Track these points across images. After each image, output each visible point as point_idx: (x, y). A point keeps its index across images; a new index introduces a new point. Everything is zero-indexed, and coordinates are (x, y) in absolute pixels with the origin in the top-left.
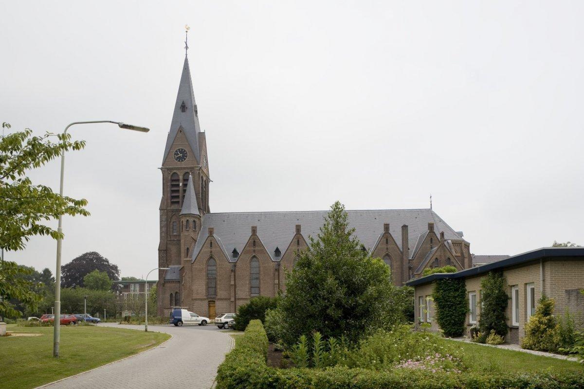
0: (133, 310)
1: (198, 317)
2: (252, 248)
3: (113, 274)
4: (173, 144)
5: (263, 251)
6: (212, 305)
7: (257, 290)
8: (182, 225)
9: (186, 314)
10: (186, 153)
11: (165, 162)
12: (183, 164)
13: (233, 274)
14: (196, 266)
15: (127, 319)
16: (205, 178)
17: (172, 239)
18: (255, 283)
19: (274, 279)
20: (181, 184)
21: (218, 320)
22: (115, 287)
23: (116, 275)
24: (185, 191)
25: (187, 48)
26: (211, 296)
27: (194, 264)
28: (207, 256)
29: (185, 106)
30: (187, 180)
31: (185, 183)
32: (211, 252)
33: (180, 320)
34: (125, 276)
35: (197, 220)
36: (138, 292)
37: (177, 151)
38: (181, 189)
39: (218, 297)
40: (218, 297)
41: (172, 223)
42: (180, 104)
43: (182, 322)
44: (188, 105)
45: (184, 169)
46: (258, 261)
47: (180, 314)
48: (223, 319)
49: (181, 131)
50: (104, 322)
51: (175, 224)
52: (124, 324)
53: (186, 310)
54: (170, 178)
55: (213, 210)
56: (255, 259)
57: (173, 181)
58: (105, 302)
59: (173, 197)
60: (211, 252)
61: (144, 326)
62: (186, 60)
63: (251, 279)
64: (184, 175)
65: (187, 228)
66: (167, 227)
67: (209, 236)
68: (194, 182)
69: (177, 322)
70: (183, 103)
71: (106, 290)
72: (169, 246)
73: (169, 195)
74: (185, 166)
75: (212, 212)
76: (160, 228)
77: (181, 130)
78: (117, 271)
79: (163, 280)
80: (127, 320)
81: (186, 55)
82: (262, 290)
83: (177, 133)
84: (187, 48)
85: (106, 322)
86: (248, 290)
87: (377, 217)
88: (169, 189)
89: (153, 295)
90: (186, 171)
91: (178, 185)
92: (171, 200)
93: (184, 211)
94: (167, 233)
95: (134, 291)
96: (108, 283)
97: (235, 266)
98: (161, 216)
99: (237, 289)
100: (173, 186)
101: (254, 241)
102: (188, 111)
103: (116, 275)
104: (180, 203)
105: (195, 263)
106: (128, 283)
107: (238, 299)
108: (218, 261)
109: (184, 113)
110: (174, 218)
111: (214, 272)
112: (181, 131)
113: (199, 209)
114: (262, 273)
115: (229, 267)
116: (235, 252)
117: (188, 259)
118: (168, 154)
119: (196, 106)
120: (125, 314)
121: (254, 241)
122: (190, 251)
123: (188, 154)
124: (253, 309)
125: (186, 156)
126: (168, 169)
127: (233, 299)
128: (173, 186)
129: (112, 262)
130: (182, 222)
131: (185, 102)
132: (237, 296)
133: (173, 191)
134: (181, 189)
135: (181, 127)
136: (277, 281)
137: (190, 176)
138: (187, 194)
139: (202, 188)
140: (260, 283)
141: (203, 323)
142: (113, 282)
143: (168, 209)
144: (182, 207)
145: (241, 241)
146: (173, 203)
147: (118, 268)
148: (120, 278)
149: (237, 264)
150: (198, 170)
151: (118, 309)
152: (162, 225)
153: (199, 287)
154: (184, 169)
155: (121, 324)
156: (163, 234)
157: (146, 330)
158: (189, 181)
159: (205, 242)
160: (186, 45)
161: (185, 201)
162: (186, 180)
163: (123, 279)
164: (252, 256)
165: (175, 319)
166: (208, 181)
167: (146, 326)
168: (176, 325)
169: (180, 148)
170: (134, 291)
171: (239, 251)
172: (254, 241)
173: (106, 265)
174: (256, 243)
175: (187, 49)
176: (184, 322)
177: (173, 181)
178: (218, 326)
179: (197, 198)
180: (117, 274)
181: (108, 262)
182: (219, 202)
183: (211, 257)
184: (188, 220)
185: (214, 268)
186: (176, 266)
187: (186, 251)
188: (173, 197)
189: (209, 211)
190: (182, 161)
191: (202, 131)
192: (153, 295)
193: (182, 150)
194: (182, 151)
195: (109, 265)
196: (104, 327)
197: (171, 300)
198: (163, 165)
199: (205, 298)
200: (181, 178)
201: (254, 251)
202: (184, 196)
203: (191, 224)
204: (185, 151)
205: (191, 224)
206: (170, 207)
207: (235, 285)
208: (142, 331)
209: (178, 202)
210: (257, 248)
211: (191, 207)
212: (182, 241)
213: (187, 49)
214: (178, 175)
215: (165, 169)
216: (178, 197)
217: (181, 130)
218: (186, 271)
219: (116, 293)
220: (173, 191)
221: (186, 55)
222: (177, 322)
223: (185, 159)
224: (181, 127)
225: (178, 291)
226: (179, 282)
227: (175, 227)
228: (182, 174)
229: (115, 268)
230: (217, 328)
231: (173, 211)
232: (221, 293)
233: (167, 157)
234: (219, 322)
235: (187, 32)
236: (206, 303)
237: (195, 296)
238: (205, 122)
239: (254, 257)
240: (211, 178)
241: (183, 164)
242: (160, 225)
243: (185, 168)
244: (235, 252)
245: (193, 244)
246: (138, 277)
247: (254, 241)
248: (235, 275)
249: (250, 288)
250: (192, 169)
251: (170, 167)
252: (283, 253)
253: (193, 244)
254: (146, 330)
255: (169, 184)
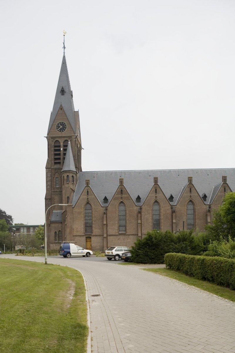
0: (23, 244)
1: (83, 249)
2: (120, 196)
3: (9, 221)
4: (55, 119)
5: (129, 198)
6: (88, 240)
7: (124, 228)
8: (64, 179)
9: (74, 248)
10: (66, 126)
11: (49, 132)
12: (64, 134)
13: (105, 216)
14: (76, 210)
15: (22, 251)
16: (79, 146)
17: (55, 190)
18: (123, 223)
19: (138, 220)
20: (62, 149)
21: (109, 253)
22: (10, 229)
23: (11, 222)
24: (65, 154)
25: (64, 47)
26: (88, 233)
27: (75, 208)
28: (85, 202)
29: (64, 91)
30: (67, 146)
31: (65, 152)
32: (88, 199)
33: (69, 253)
34: (17, 223)
35: (74, 175)
36: (26, 233)
37: (58, 124)
38: (62, 153)
39: (94, 234)
40: (94, 234)
41: (55, 178)
42: (60, 89)
43: (70, 254)
44: (66, 90)
45: (63, 138)
46: (125, 206)
47: (69, 248)
48: (114, 252)
49: (61, 109)
50: (4, 253)
51: (57, 179)
52: (20, 255)
53: (73, 244)
54: (53, 144)
55: (84, 169)
56: (122, 204)
57: (55, 146)
58: (4, 239)
59: (55, 159)
60: (88, 199)
61: (44, 258)
62: (64, 57)
63: (120, 220)
64: (64, 142)
65: (67, 181)
66: (51, 182)
67: (86, 187)
68: (72, 147)
69: (67, 254)
70: (63, 88)
71: (5, 231)
72: (53, 196)
73: (53, 157)
74: (65, 135)
75: (83, 170)
76: (46, 183)
77: (61, 108)
78: (12, 219)
79: (49, 222)
80: (21, 252)
81: (64, 53)
82: (128, 228)
83: (59, 111)
84: (64, 47)
85: (5, 253)
86: (117, 228)
87: (209, 174)
88: (52, 153)
89: (37, 234)
90: (66, 139)
91: (60, 150)
92: (54, 161)
93: (65, 168)
94: (51, 186)
95: (23, 232)
96: (6, 227)
97: (106, 210)
98: (47, 173)
99: (108, 227)
100: (55, 150)
101: (122, 190)
102: (66, 94)
103: (11, 222)
104: (61, 163)
105: (75, 207)
106: (19, 227)
107: (109, 235)
108: (93, 206)
109: (63, 96)
110: (57, 174)
111: (90, 214)
112: (61, 109)
113: (75, 167)
114: (127, 215)
115: (102, 210)
116: (106, 199)
117: (69, 204)
118: (52, 126)
119: (71, 92)
120: (17, 248)
121: (122, 190)
122: (71, 198)
123: (67, 126)
124: (152, 242)
125: (66, 128)
126: (52, 138)
127: (105, 235)
128: (55, 150)
129: (8, 213)
130: (64, 177)
131: (64, 87)
132: (108, 234)
133: (56, 155)
134: (62, 153)
135: (61, 106)
136: (140, 221)
137: (69, 142)
138: (67, 157)
139: (77, 153)
140: (126, 222)
141: (88, 255)
142: (9, 226)
143: (52, 167)
144: (63, 166)
145: (111, 190)
146: (55, 163)
147: (12, 218)
148: (14, 224)
149: (108, 208)
150: (74, 138)
151: (13, 244)
152: (48, 180)
153: (79, 226)
154: (63, 138)
155: (17, 255)
156: (48, 187)
157: (46, 263)
158: (68, 146)
159: (83, 191)
160: (64, 45)
161: (65, 161)
162: (66, 146)
163: (15, 224)
164: (119, 202)
165: (65, 251)
166: (81, 149)
167: (46, 259)
168: (65, 256)
169: (61, 121)
170: (23, 232)
171: (109, 198)
172: (122, 190)
173: (4, 215)
174: (123, 192)
175: (64, 49)
176: (72, 254)
177: (55, 146)
178: (108, 258)
179: (74, 160)
180: (11, 221)
181: (5, 213)
182: (88, 164)
183: (88, 203)
184: (68, 176)
185: (90, 211)
186: (59, 211)
187: (67, 199)
188: (55, 159)
189: (81, 171)
190: (63, 131)
191: (76, 110)
192: (37, 234)
193: (62, 123)
194: (63, 124)
195: (6, 216)
196: (5, 259)
197: (55, 237)
198: (48, 135)
199: (84, 235)
200: (62, 144)
201: (122, 198)
202: (64, 162)
203: (71, 179)
204: (64, 124)
205: (71, 179)
206: (54, 166)
207: (107, 225)
208: (42, 264)
209: (59, 163)
210: (123, 196)
211: (70, 165)
212: (63, 192)
213: (64, 49)
214: (60, 143)
215: (50, 138)
216: (59, 159)
217: (61, 108)
218: (68, 213)
219: (11, 233)
220: (56, 155)
221: (64, 53)
222: (66, 254)
223: (64, 130)
224: (61, 106)
225: (60, 230)
226: (62, 223)
227: (57, 182)
228: (63, 141)
229: (10, 217)
230: (107, 259)
231: (56, 169)
232: (96, 231)
233: (51, 129)
234: (111, 254)
235: (64, 35)
236: (84, 238)
237: (75, 233)
238: (78, 104)
239: (122, 202)
240: (83, 146)
241: (64, 134)
242: (46, 180)
243: (64, 137)
244: (106, 199)
245: (72, 193)
246: (25, 223)
247: (122, 190)
248: (107, 217)
249: (118, 226)
250: (70, 137)
251: (53, 136)
252: (142, 200)
253: (72, 193)
254: (46, 263)
255: (53, 149)
